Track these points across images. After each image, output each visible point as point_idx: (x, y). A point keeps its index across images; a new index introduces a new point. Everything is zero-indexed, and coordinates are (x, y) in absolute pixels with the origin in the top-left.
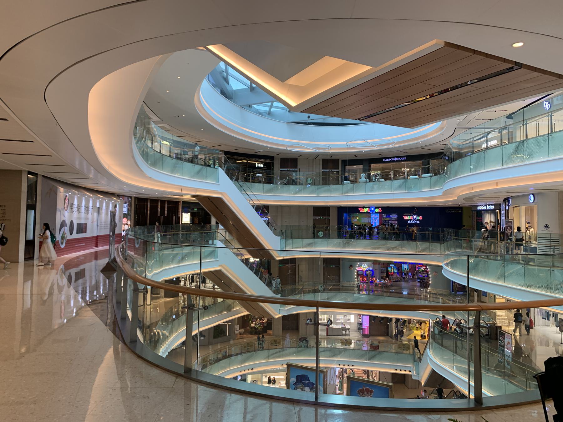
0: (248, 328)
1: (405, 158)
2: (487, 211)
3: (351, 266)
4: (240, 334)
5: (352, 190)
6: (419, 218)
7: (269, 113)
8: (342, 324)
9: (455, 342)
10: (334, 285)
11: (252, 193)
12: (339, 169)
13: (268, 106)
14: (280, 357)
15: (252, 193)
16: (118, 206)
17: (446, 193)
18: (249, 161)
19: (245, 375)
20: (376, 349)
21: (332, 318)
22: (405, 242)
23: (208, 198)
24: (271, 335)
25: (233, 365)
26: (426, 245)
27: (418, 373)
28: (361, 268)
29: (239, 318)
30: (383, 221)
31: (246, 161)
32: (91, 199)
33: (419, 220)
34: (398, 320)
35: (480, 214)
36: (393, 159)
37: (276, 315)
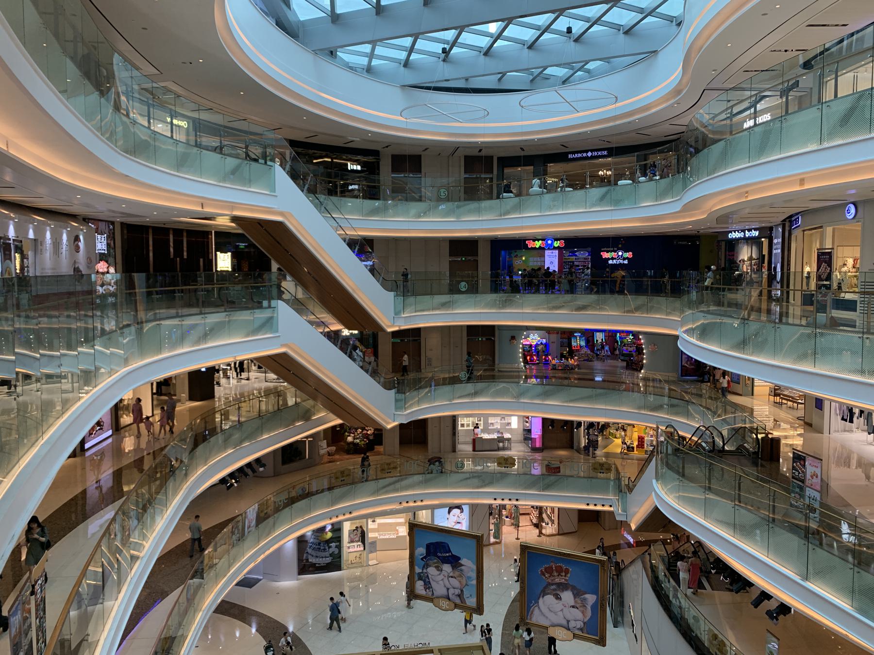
0: (342, 443)
1: (605, 153)
2: (747, 240)
3: (513, 338)
4: (329, 454)
5: (518, 208)
6: (626, 255)
7: (369, 70)
8: (499, 432)
9: (707, 471)
10: (485, 370)
11: (341, 216)
12: (492, 172)
13: (364, 55)
14: (397, 490)
15: (341, 216)
16: (81, 237)
17: (688, 208)
18: (335, 159)
19: (340, 523)
20: (555, 473)
21: (482, 422)
22: (608, 296)
23: (259, 223)
24: (382, 455)
25: (315, 509)
26: (642, 299)
27: (624, 510)
28: (528, 341)
29: (325, 430)
30: (564, 262)
31: (330, 160)
32: (11, 222)
33: (627, 258)
34: (591, 425)
35: (732, 245)
36: (585, 155)
37: (388, 423)
